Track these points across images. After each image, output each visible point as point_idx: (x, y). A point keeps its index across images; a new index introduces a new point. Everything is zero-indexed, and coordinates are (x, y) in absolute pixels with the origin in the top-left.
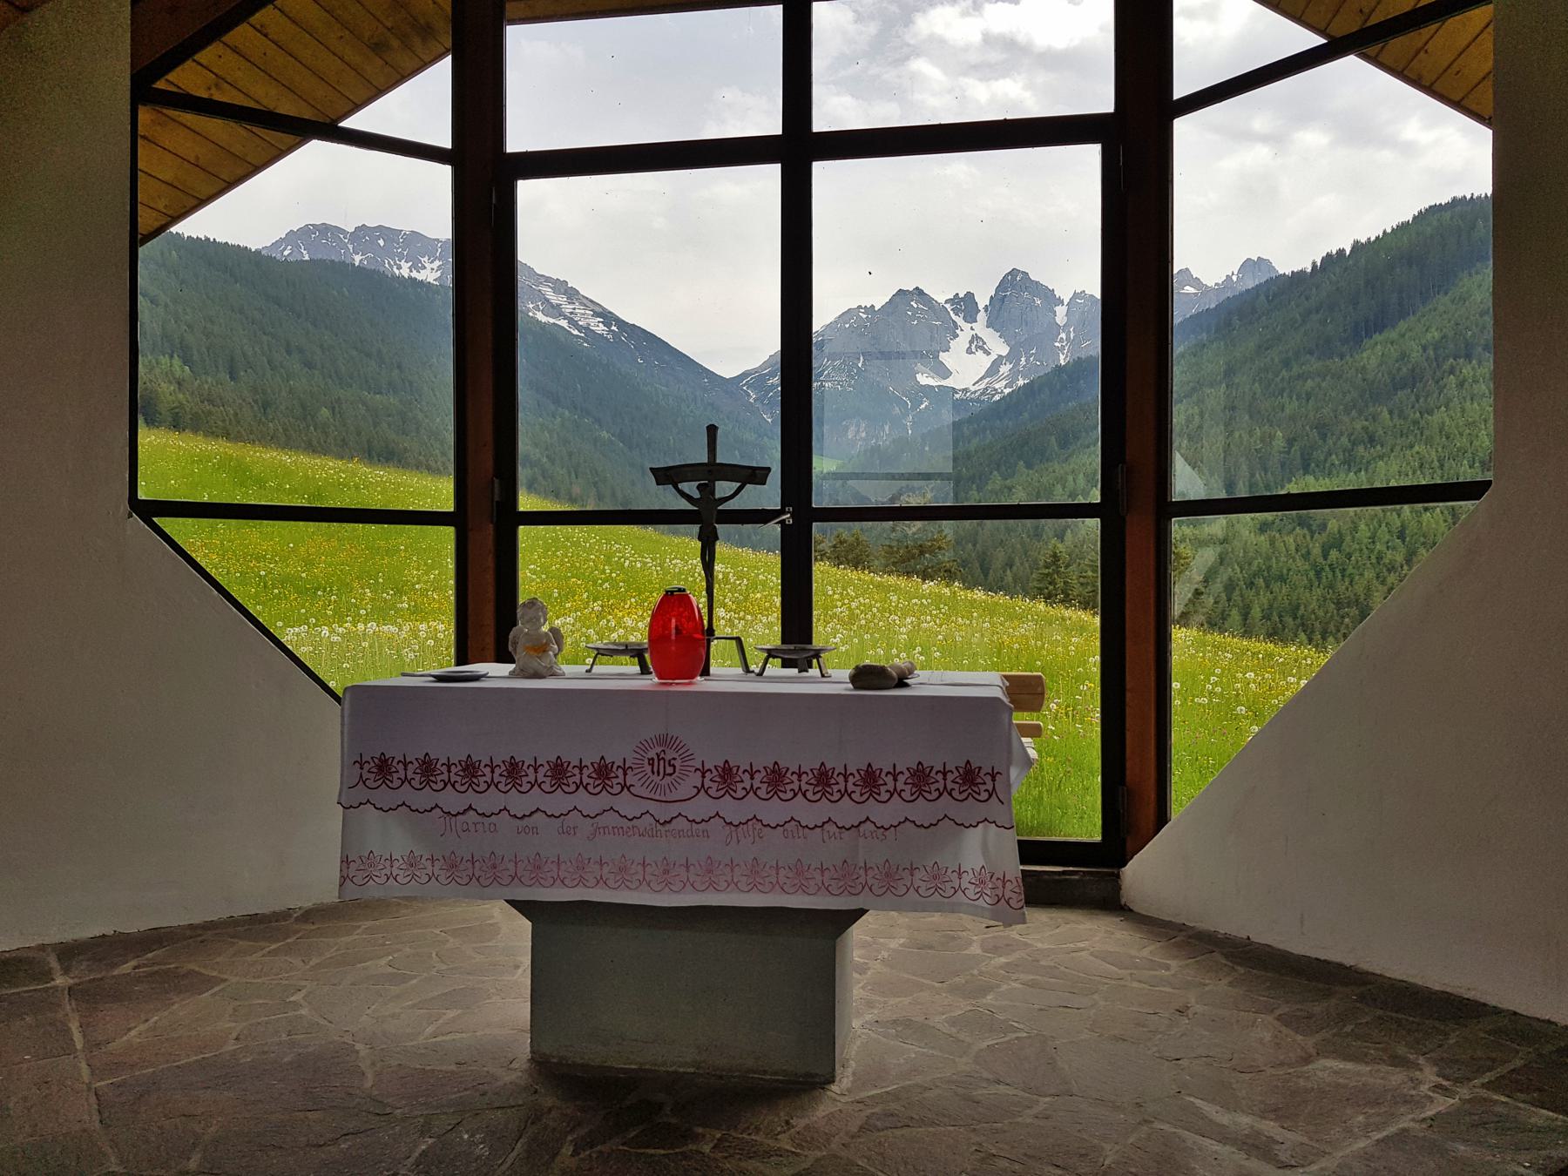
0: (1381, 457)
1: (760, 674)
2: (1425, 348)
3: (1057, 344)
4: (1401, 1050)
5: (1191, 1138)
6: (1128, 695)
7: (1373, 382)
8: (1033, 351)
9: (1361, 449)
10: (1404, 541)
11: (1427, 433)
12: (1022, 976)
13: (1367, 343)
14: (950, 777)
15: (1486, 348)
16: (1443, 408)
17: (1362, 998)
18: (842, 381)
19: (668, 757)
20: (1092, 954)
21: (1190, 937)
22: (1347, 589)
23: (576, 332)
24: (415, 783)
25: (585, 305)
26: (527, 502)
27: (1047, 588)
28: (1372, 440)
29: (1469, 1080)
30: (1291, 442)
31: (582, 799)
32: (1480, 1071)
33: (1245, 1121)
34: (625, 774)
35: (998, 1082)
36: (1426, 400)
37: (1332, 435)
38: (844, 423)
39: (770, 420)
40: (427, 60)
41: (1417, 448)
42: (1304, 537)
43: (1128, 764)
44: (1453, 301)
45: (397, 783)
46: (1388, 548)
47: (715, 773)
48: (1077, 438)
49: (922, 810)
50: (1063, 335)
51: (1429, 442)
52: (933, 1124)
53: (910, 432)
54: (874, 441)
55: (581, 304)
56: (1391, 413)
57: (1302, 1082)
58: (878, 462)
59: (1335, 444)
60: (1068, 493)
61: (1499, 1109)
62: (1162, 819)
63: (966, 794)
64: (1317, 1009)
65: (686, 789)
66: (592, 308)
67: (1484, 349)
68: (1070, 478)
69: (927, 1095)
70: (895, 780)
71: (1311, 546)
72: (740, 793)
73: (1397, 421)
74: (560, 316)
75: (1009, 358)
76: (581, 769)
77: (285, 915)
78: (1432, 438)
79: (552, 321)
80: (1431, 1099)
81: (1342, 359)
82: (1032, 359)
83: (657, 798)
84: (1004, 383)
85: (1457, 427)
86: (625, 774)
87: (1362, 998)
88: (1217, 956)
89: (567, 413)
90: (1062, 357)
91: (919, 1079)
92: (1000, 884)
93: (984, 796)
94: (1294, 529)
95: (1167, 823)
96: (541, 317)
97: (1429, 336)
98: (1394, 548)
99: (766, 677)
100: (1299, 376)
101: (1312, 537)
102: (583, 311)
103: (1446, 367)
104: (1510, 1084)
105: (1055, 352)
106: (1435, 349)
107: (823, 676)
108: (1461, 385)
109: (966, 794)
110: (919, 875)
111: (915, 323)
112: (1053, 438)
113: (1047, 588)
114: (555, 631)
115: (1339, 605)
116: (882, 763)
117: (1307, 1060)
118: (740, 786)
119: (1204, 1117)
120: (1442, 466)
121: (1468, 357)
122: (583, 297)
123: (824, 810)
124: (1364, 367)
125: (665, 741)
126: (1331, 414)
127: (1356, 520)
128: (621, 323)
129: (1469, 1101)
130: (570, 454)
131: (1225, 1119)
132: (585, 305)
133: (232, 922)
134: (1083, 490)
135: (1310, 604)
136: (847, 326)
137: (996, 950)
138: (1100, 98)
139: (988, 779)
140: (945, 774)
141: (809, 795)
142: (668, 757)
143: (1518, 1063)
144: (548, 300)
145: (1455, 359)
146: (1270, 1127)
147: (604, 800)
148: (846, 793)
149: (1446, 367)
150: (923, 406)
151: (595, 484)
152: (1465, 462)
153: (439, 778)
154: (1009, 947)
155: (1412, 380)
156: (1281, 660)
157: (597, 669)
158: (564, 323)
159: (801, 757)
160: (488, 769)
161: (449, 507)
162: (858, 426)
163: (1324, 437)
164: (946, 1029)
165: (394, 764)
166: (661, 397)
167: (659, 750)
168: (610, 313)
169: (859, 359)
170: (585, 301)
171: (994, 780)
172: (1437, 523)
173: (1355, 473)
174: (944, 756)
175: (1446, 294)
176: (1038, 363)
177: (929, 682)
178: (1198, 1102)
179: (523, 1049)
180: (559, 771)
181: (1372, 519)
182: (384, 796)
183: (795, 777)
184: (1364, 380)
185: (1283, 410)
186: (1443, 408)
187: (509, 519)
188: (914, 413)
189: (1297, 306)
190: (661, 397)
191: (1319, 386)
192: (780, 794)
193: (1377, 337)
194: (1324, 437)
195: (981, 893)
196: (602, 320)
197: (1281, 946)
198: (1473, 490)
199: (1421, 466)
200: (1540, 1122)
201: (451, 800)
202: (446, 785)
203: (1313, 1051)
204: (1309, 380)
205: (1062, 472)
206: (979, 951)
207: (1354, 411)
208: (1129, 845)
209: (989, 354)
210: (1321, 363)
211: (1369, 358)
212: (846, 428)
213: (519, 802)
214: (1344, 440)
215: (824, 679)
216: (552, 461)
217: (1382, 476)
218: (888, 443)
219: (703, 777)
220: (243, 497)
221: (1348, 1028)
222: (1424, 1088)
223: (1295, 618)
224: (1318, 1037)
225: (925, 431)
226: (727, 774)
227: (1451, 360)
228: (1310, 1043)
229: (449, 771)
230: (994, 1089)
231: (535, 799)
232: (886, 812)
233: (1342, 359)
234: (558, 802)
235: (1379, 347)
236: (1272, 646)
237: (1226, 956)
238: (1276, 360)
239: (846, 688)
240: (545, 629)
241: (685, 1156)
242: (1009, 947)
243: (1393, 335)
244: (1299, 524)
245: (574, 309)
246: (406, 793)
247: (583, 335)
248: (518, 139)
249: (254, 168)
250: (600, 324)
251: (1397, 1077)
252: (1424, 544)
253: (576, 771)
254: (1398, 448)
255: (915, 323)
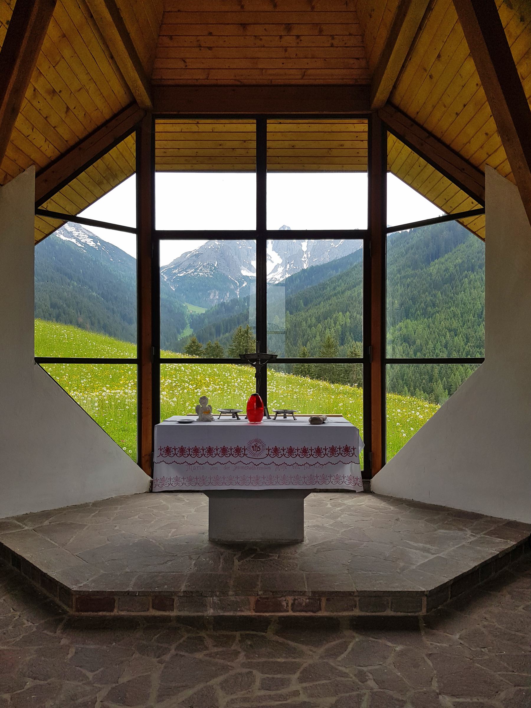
0: (438, 312)
1: (275, 419)
2: (455, 266)
3: (303, 259)
4: (461, 527)
5: (408, 549)
6: (372, 422)
7: (434, 280)
8: (293, 262)
9: (429, 308)
10: (447, 349)
11: (456, 302)
12: (347, 513)
13: (432, 263)
14: (341, 450)
15: (480, 267)
16: (463, 292)
17: (448, 514)
18: (207, 272)
19: (258, 446)
20: (366, 506)
21: (394, 500)
22: (424, 367)
23: (80, 245)
24: (220, 455)
25: (84, 232)
26: (164, 354)
27: (301, 368)
28: (434, 305)
29: (480, 533)
30: (401, 305)
31: (231, 458)
32: (483, 531)
33: (421, 545)
34: (245, 451)
35: (351, 539)
36: (456, 289)
37: (418, 302)
38: (208, 292)
39: (174, 289)
40: (113, 186)
41: (452, 308)
42: (407, 347)
43: (372, 445)
44: (467, 247)
45: (172, 455)
46: (440, 352)
47: (272, 450)
48: (311, 301)
49: (333, 459)
50: (305, 255)
51: (457, 306)
52: (336, 550)
53: (238, 296)
54: (222, 300)
55: (82, 232)
56: (442, 294)
57: (435, 536)
58: (224, 310)
59: (419, 306)
60: (308, 325)
61: (487, 539)
62: (383, 463)
63: (346, 455)
64: (436, 518)
65: (264, 454)
66: (88, 234)
67: (479, 268)
68: (309, 319)
69: (332, 543)
70: (326, 451)
71: (409, 350)
72: (280, 456)
73: (445, 297)
74: (72, 237)
75: (282, 265)
76: (340, 449)
77: (86, 505)
78: (458, 304)
79: (68, 239)
80: (470, 538)
81: (422, 270)
82: (292, 265)
83: (255, 457)
84: (280, 275)
85: (468, 300)
86: (245, 451)
87: (448, 514)
88: (404, 505)
89: (75, 283)
90: (305, 265)
91: (327, 540)
92: (356, 479)
93: (351, 455)
94: (402, 343)
95: (385, 465)
96: (64, 238)
97: (457, 261)
98: (443, 352)
99: (277, 420)
100: (404, 277)
101: (410, 347)
102: (83, 235)
103: (464, 274)
104: (490, 533)
105: (302, 262)
106: (460, 267)
107: (295, 420)
108: (470, 283)
109: (346, 455)
110: (332, 478)
111: (241, 247)
112: (301, 301)
113: (301, 368)
114: (210, 406)
115: (421, 374)
116: (322, 446)
117: (436, 530)
118: (280, 454)
119: (409, 545)
120: (462, 316)
121: (473, 271)
122: (83, 228)
123: (305, 460)
124: (431, 274)
125: (257, 441)
126: (418, 294)
127: (427, 339)
128: (103, 242)
129: (480, 538)
130: (77, 303)
131: (416, 545)
132: (84, 232)
133: (68, 508)
134: (314, 324)
135: (409, 374)
136: (210, 247)
137: (335, 506)
138: (363, 225)
139: (352, 450)
140: (340, 449)
141: (301, 456)
142: (258, 446)
143: (492, 528)
144: (66, 230)
145: (467, 271)
146: (428, 546)
147: (238, 459)
148: (311, 455)
149: (464, 274)
150: (244, 285)
151: (90, 317)
152: (471, 315)
153: (186, 453)
154: (340, 505)
155: (451, 279)
156: (405, 402)
157: (221, 418)
158: (74, 241)
159: (298, 445)
160: (202, 450)
161: (135, 357)
162: (215, 293)
163: (414, 303)
164: (330, 527)
165: (172, 449)
166: (122, 277)
167: (255, 443)
168: (97, 236)
169: (215, 263)
170: (84, 231)
171: (354, 450)
172: (460, 341)
173: (427, 319)
174: (340, 444)
175: (464, 243)
176: (295, 268)
177: (332, 422)
178: (407, 541)
179: (206, 536)
180: (224, 450)
181: (434, 340)
182: (168, 459)
183: (296, 451)
184: (431, 279)
185: (398, 292)
186: (463, 292)
187: (157, 361)
188: (240, 288)
189: (404, 246)
190: (122, 277)
191: (412, 281)
192: (292, 456)
193: (436, 261)
194: (414, 303)
195: (350, 483)
196: (92, 240)
197: (423, 501)
198: (480, 361)
199: (454, 316)
200: (498, 541)
201: (190, 460)
202: (188, 455)
203: (436, 528)
204: (409, 279)
205: (306, 316)
206: (330, 506)
207: (427, 293)
208: (373, 471)
209: (273, 262)
210: (413, 272)
211: (433, 270)
212: (209, 294)
213: (212, 460)
214: (423, 305)
215: (295, 421)
216: (69, 306)
217: (438, 320)
218: (229, 301)
219: (269, 451)
220: (121, 366)
221: (446, 522)
222: (468, 536)
223: (403, 380)
224: (437, 525)
225: (245, 296)
226: (276, 450)
227: (466, 272)
228: (435, 526)
229: (189, 451)
230: (350, 541)
231: (217, 459)
232: (322, 460)
233: (422, 270)
234: (224, 460)
235: (437, 265)
236: (400, 396)
237: (407, 505)
238: (395, 269)
239: (308, 424)
240: (207, 406)
241: (271, 560)
242: (340, 505)
243: (442, 260)
244: (404, 341)
245: (79, 234)
246: (175, 458)
247: (83, 246)
248: (159, 226)
249: (54, 228)
250: (92, 242)
251: (460, 533)
252: (455, 350)
253: (230, 450)
254: (444, 308)
255: (241, 247)
